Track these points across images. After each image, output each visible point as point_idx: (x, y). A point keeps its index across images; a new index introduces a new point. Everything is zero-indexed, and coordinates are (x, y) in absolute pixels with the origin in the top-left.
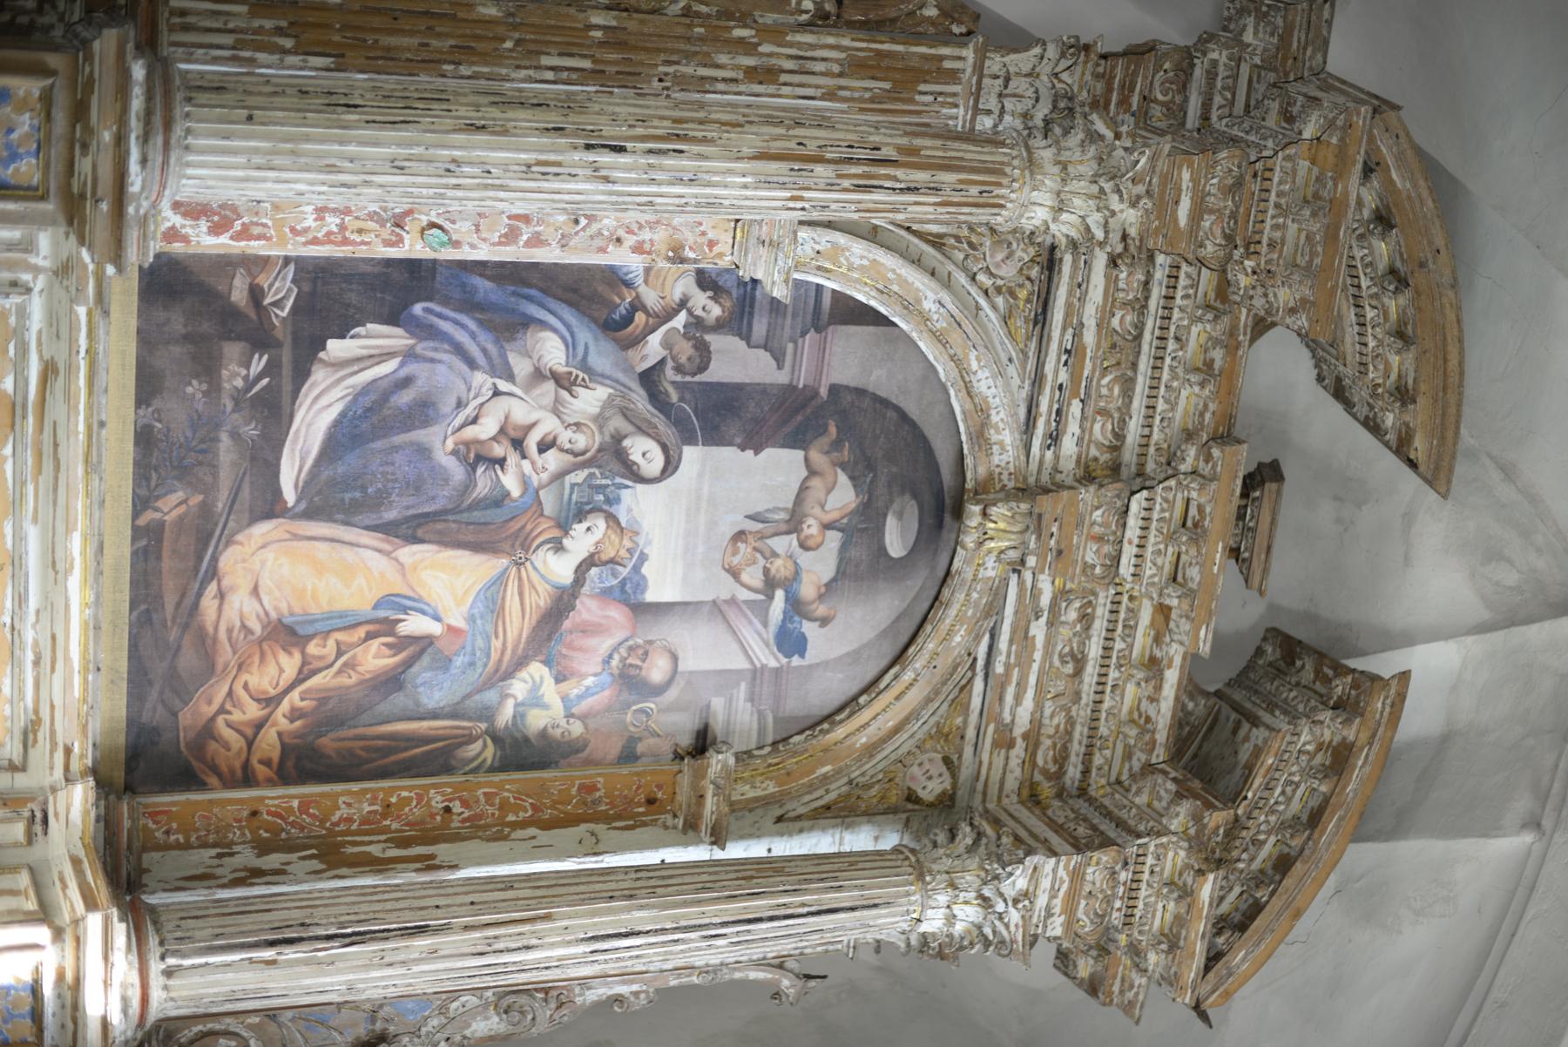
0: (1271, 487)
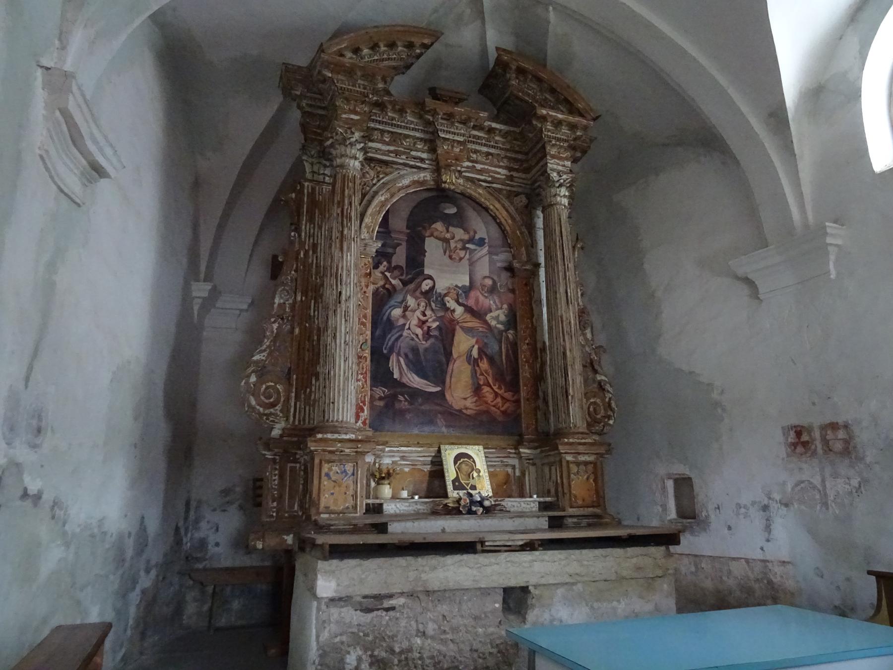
0: (438, 92)
